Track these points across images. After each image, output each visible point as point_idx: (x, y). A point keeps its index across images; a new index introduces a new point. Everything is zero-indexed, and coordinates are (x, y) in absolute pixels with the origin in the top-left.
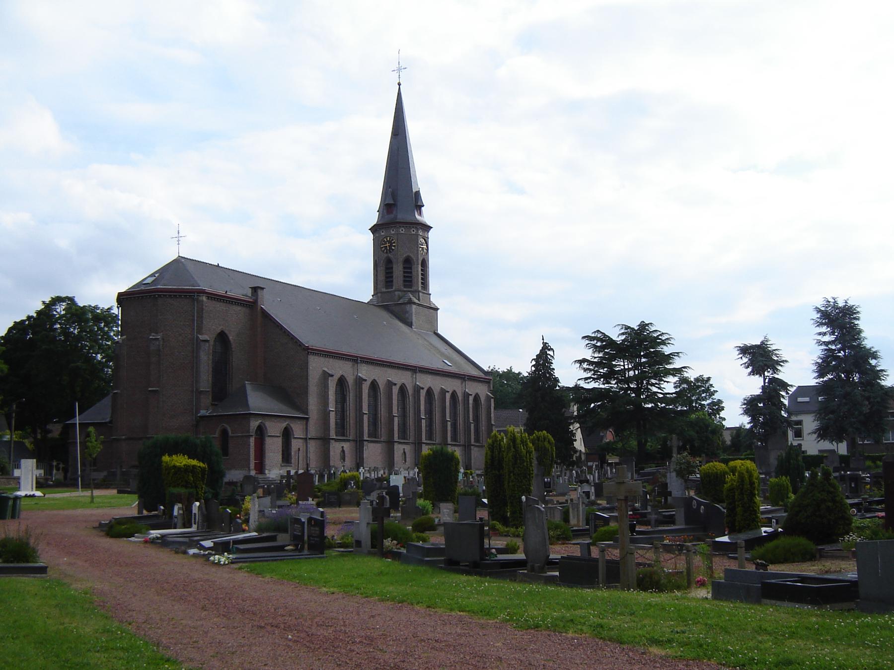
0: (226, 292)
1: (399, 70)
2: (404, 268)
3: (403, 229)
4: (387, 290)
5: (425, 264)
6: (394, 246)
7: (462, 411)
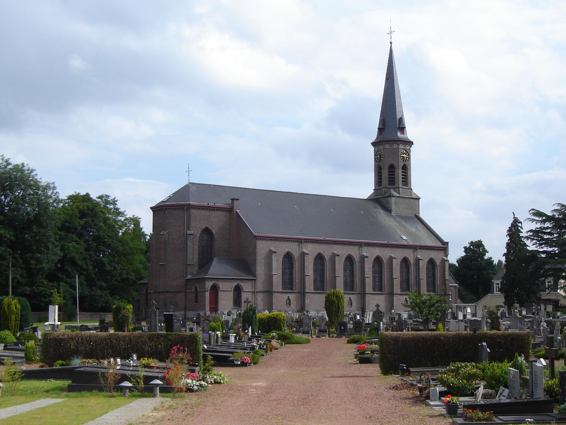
0: (208, 204)
1: (391, 33)
2: (389, 172)
3: (388, 145)
4: (379, 188)
5: (406, 169)
6: (382, 157)
7: (413, 273)
